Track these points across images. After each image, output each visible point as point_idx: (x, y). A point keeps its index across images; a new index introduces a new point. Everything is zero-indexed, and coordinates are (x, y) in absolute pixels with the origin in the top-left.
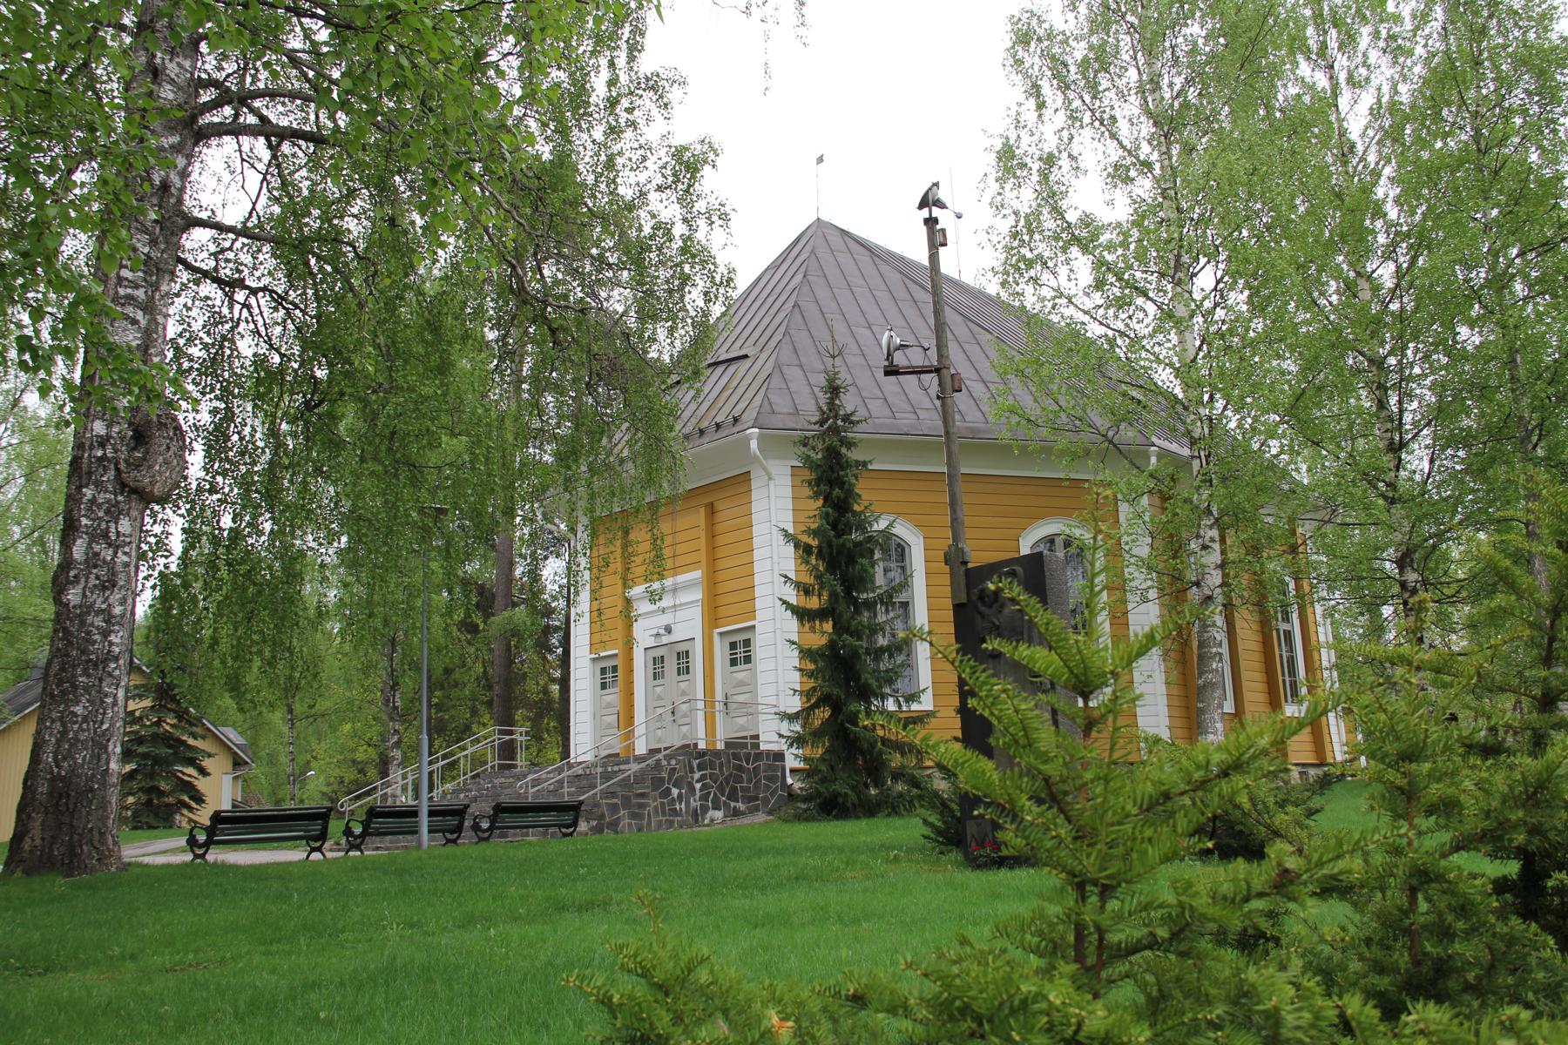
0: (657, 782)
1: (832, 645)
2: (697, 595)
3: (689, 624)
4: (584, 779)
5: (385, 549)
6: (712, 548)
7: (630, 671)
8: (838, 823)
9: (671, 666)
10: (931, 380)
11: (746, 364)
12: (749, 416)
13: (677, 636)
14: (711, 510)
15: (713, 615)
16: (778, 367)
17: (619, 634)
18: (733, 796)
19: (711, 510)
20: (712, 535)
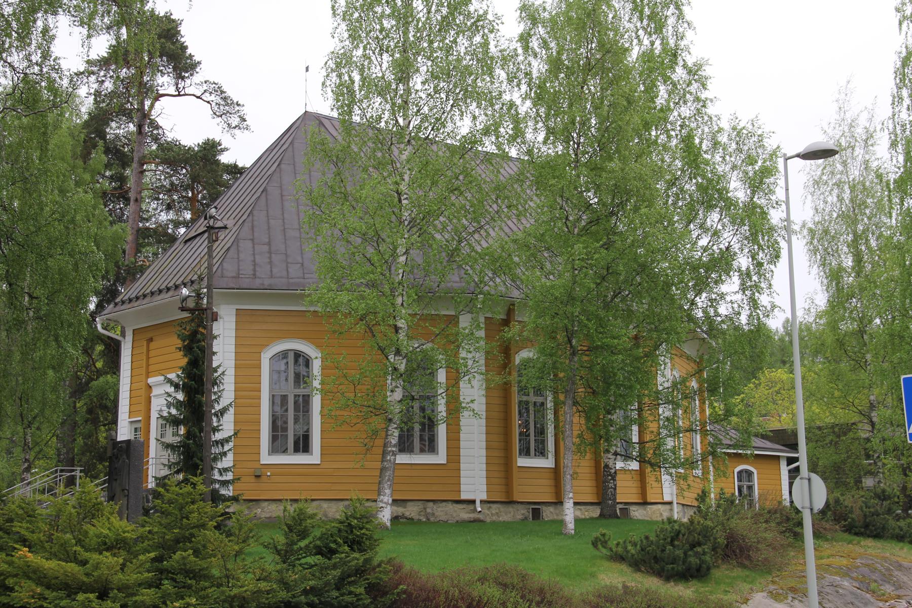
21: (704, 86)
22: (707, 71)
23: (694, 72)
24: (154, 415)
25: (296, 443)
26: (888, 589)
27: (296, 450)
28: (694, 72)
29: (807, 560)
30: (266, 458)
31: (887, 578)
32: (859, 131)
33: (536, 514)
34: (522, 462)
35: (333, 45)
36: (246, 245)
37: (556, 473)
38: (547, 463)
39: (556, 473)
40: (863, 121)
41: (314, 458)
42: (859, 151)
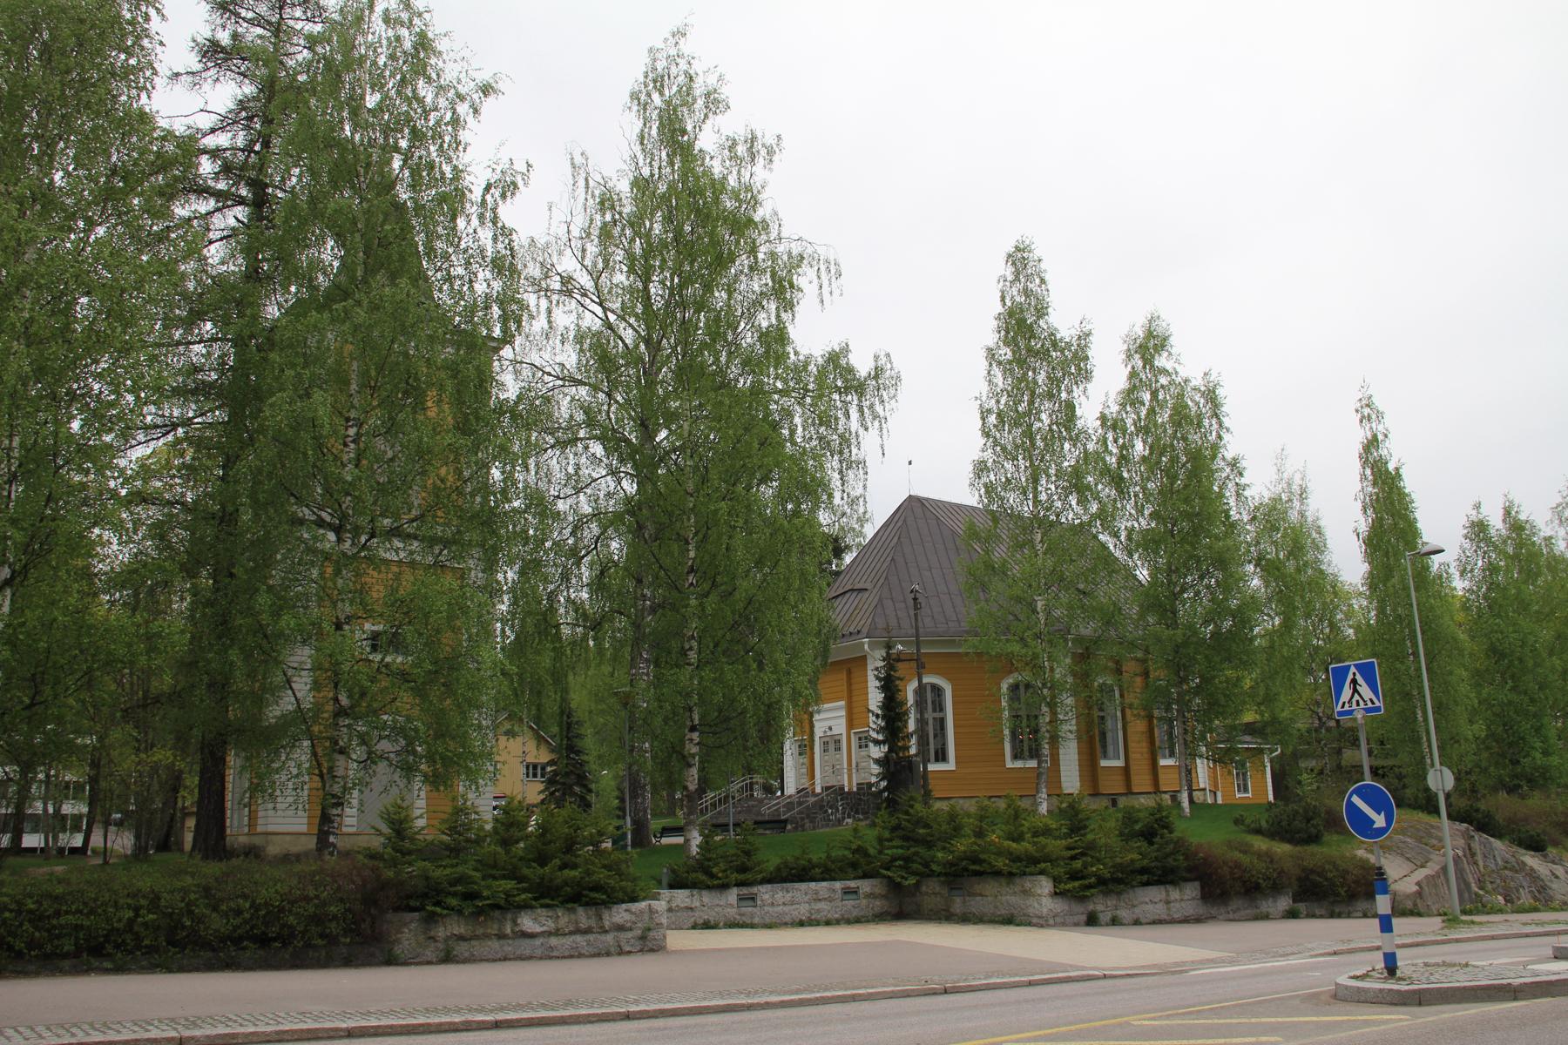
0: (822, 807)
1: (886, 757)
2: (843, 713)
3: (840, 728)
4: (790, 806)
5: (352, 431)
6: (850, 691)
7: (812, 748)
8: (1151, 944)
9: (832, 747)
10: (914, 664)
11: (866, 594)
12: (865, 631)
13: (835, 732)
14: (849, 672)
15: (851, 724)
16: (880, 600)
17: (807, 728)
18: (857, 812)
19: (849, 672)
20: (850, 684)
21: (1241, 474)
22: (1243, 464)
23: (1234, 464)
24: (817, 739)
25: (936, 753)
26: (1434, 842)
27: (937, 760)
28: (1234, 464)
29: (632, 958)
30: (1009, 764)
31: (1430, 835)
32: (1295, 487)
33: (1114, 803)
34: (1104, 763)
35: (976, 455)
36: (888, 603)
37: (1126, 770)
38: (1120, 763)
39: (1126, 770)
40: (1297, 480)
41: (951, 765)
42: (1296, 504)
